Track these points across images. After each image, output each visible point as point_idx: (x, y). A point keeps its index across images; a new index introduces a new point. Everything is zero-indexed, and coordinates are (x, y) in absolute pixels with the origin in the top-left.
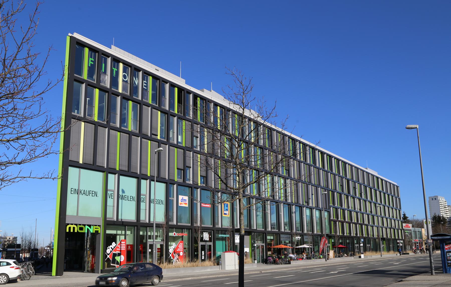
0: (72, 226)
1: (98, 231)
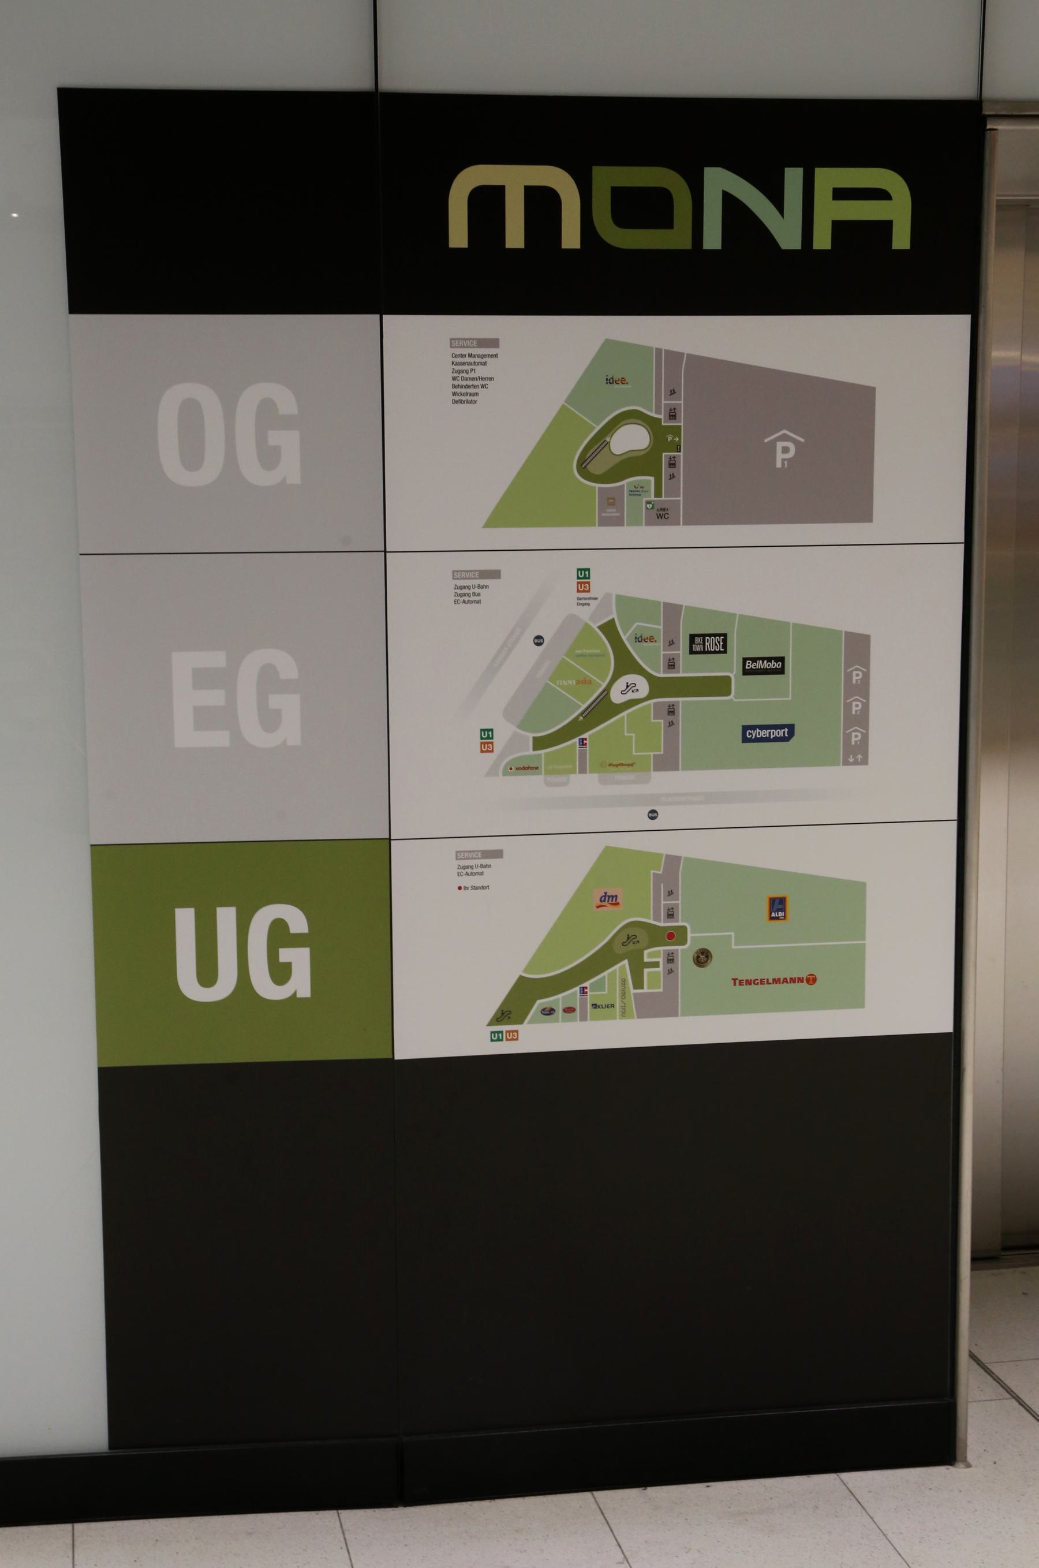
0: (515, 179)
1: (886, 227)
